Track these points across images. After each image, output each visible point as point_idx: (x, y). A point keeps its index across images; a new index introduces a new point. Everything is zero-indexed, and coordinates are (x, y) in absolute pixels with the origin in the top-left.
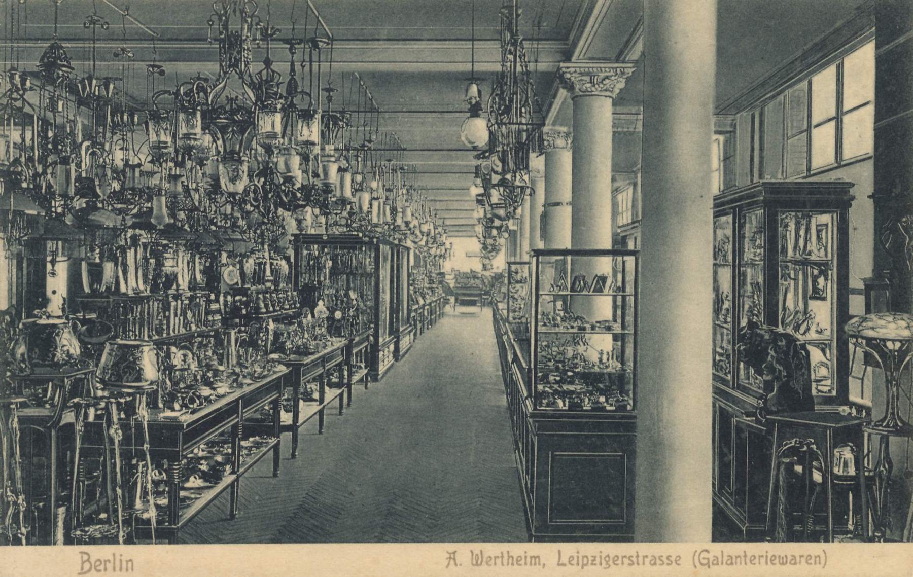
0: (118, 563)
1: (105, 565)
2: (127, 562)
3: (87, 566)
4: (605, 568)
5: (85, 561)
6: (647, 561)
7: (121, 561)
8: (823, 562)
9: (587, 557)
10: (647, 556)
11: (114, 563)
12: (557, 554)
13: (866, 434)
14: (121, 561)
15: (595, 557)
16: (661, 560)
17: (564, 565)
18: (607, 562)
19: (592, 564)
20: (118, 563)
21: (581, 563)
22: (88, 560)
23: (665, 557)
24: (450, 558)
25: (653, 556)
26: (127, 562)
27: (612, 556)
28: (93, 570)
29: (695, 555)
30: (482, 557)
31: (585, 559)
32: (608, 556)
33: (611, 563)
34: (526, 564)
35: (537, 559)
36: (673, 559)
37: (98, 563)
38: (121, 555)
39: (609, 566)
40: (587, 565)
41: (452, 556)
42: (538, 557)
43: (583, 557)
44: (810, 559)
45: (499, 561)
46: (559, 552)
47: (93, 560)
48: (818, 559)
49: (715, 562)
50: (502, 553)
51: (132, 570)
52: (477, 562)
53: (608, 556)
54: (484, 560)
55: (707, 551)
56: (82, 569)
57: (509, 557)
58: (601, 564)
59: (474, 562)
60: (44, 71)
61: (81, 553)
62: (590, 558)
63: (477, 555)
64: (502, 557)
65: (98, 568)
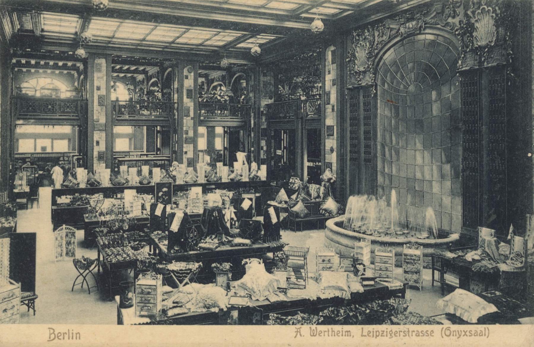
0: (71, 335)
1: (64, 335)
2: (76, 334)
3: (53, 336)
4: (390, 338)
5: (52, 334)
6: (414, 334)
7: (73, 333)
8: (487, 334)
9: (378, 331)
10: (414, 331)
11: (69, 335)
12: (361, 330)
13: (61, 227)
14: (73, 333)
15: (384, 331)
16: (423, 334)
17: (365, 336)
18: (391, 334)
19: (382, 336)
20: (71, 335)
21: (375, 335)
22: (54, 333)
23: (425, 331)
24: (297, 331)
25: (417, 331)
26: (76, 334)
27: (394, 331)
28: (56, 338)
29: (442, 330)
30: (317, 332)
31: (378, 333)
32: (391, 331)
33: (393, 335)
34: (342, 335)
35: (349, 333)
36: (429, 333)
37: (59, 335)
38: (73, 330)
39: (392, 337)
40: (378, 336)
41: (298, 332)
42: (350, 331)
43: (376, 332)
44: (397, 333)
45: (326, 334)
46: (362, 328)
47: (56, 333)
48: (78, 335)
49: (476, 334)
50: (328, 329)
51: (80, 338)
52: (313, 334)
53: (391, 331)
54: (318, 333)
55: (450, 328)
56: (50, 338)
57: (332, 331)
58: (387, 336)
59: (312, 334)
60: (203, 94)
61: (49, 328)
62: (381, 333)
63: (313, 330)
64: (328, 331)
65: (59, 338)
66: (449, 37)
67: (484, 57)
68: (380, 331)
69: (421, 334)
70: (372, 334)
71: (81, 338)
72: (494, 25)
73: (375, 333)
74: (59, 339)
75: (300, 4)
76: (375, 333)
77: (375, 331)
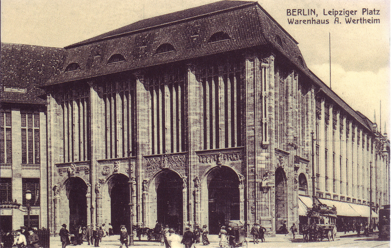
15: (341, 11)
43: (335, 11)
66: (209, 170)
67: (314, 236)
68: (339, 11)
69: (326, 22)
70: (343, 12)
71: (380, 22)
72: (348, 232)
73: (334, 12)
74: (369, 23)
75: (380, 132)
76: (334, 12)
77: (334, 11)
